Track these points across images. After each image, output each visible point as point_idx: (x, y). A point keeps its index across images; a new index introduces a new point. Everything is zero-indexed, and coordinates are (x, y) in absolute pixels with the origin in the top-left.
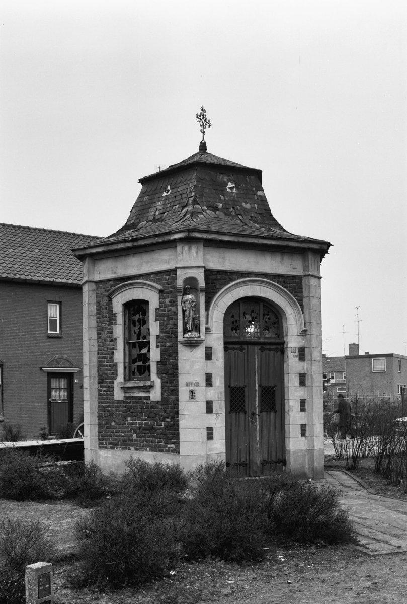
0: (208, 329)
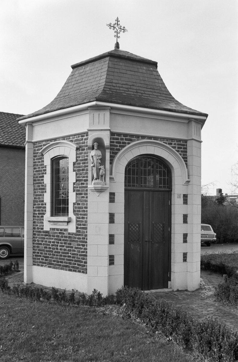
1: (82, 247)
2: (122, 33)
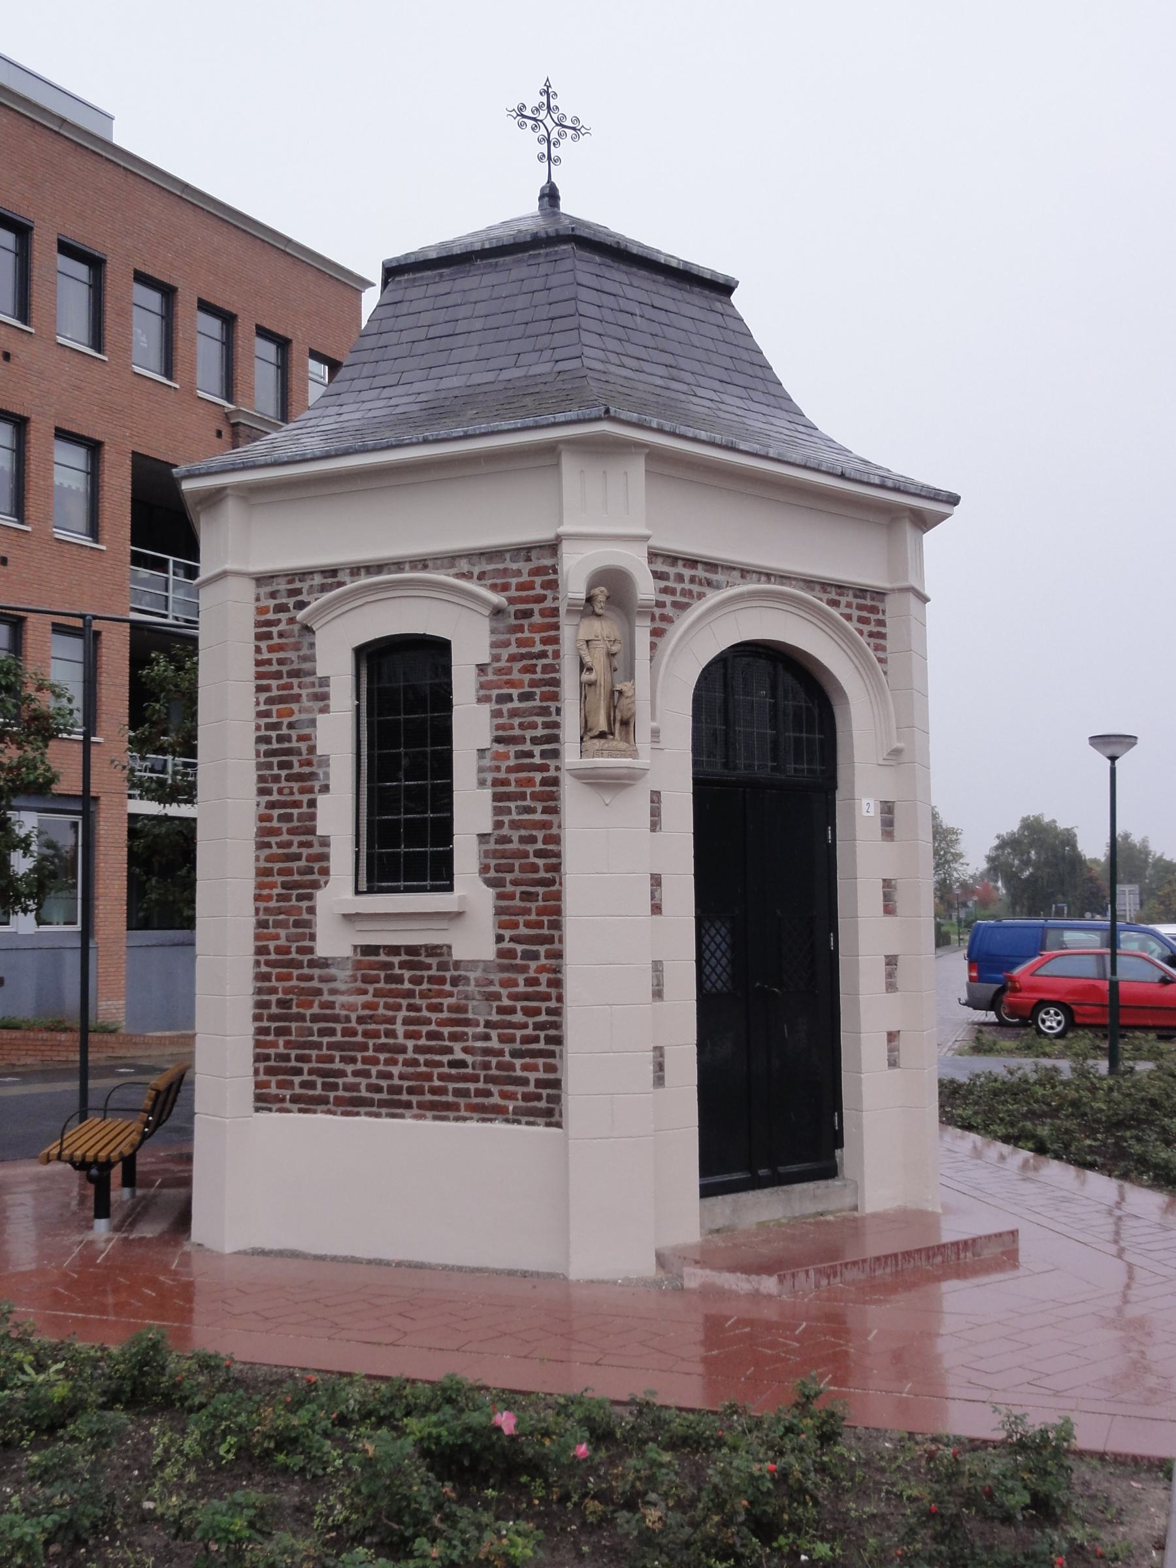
0: (655, 733)
2: (566, 142)
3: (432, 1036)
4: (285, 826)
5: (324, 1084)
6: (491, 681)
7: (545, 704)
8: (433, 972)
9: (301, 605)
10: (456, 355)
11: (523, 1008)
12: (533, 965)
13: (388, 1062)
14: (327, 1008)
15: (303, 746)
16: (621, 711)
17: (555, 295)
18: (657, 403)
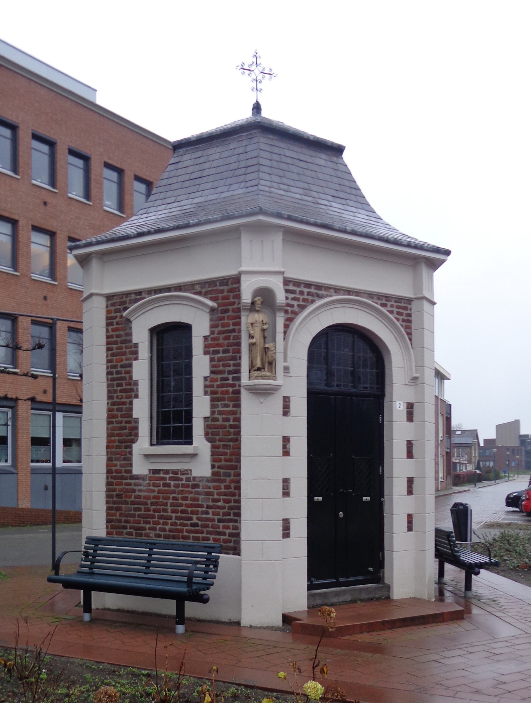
0: (286, 369)
1: (224, 504)
3: (183, 512)
4: (119, 414)
5: (136, 533)
6: (210, 344)
7: (234, 355)
8: (184, 482)
9: (125, 309)
10: (202, 187)
11: (223, 499)
12: (228, 479)
13: (164, 524)
14: (137, 498)
15: (127, 376)
16: (268, 358)
17: (250, 155)
18: (295, 207)
